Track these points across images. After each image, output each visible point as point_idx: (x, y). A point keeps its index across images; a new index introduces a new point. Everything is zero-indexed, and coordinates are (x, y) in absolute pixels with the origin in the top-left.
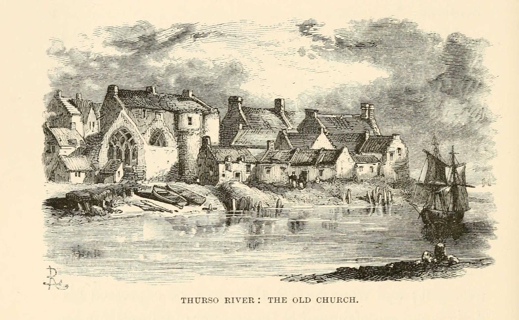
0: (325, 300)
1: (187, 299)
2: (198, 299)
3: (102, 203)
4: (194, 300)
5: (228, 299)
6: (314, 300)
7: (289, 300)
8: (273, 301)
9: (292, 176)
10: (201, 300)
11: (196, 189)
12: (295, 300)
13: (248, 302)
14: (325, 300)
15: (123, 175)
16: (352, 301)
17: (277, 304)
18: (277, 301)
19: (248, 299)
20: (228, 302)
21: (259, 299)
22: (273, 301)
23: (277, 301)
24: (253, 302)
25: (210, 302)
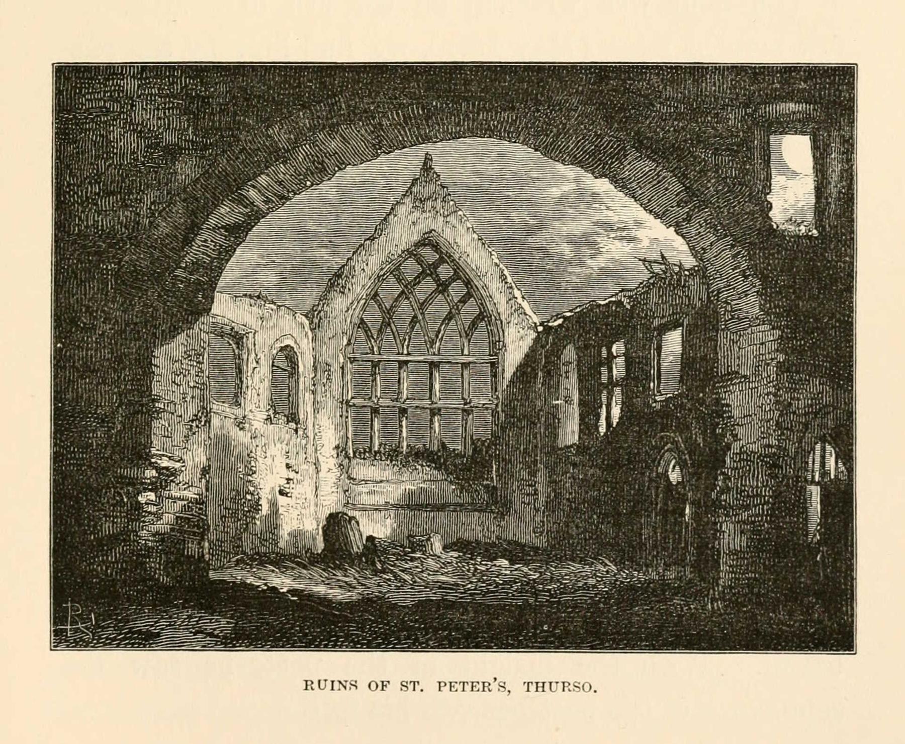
0: (540, 686)
1: (470, 684)
2: (554, 685)
3: (669, 465)
4: (547, 686)
5: (309, 683)
6: (363, 685)
7: (363, 685)
8: (533, 688)
9: (755, 275)
10: (560, 685)
11: (500, 357)
12: (373, 686)
13: (481, 689)
14: (540, 686)
15: (307, 322)
16: (540, 685)
17: (540, 693)
18: (540, 689)
19: (481, 684)
20: (309, 687)
21: (495, 679)
22: (533, 688)
23: (540, 689)
24: (490, 690)
25: (577, 689)
